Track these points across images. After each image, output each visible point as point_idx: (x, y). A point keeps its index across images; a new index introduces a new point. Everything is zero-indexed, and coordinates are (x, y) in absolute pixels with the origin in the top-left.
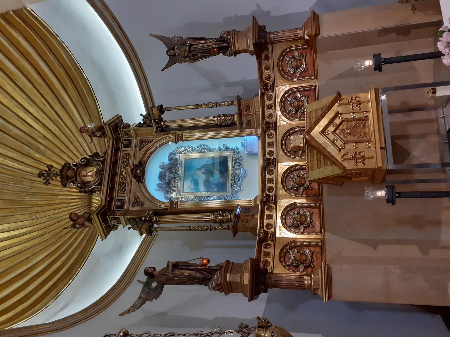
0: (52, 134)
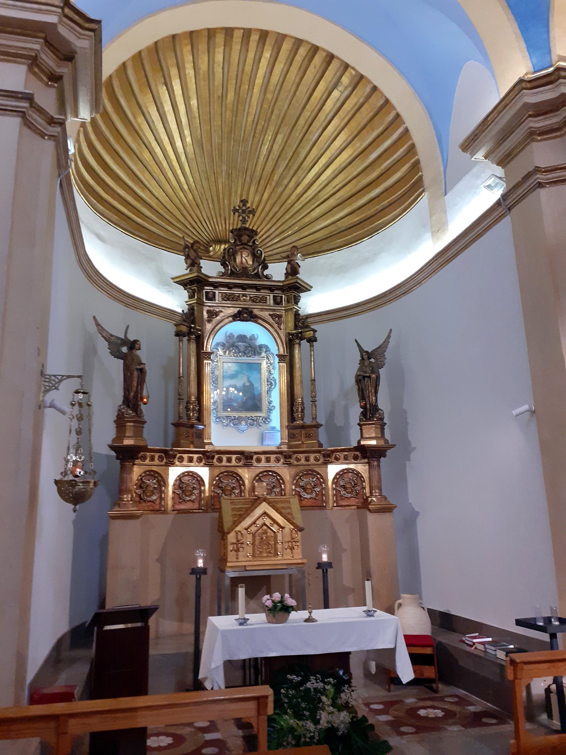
0: (301, 193)
